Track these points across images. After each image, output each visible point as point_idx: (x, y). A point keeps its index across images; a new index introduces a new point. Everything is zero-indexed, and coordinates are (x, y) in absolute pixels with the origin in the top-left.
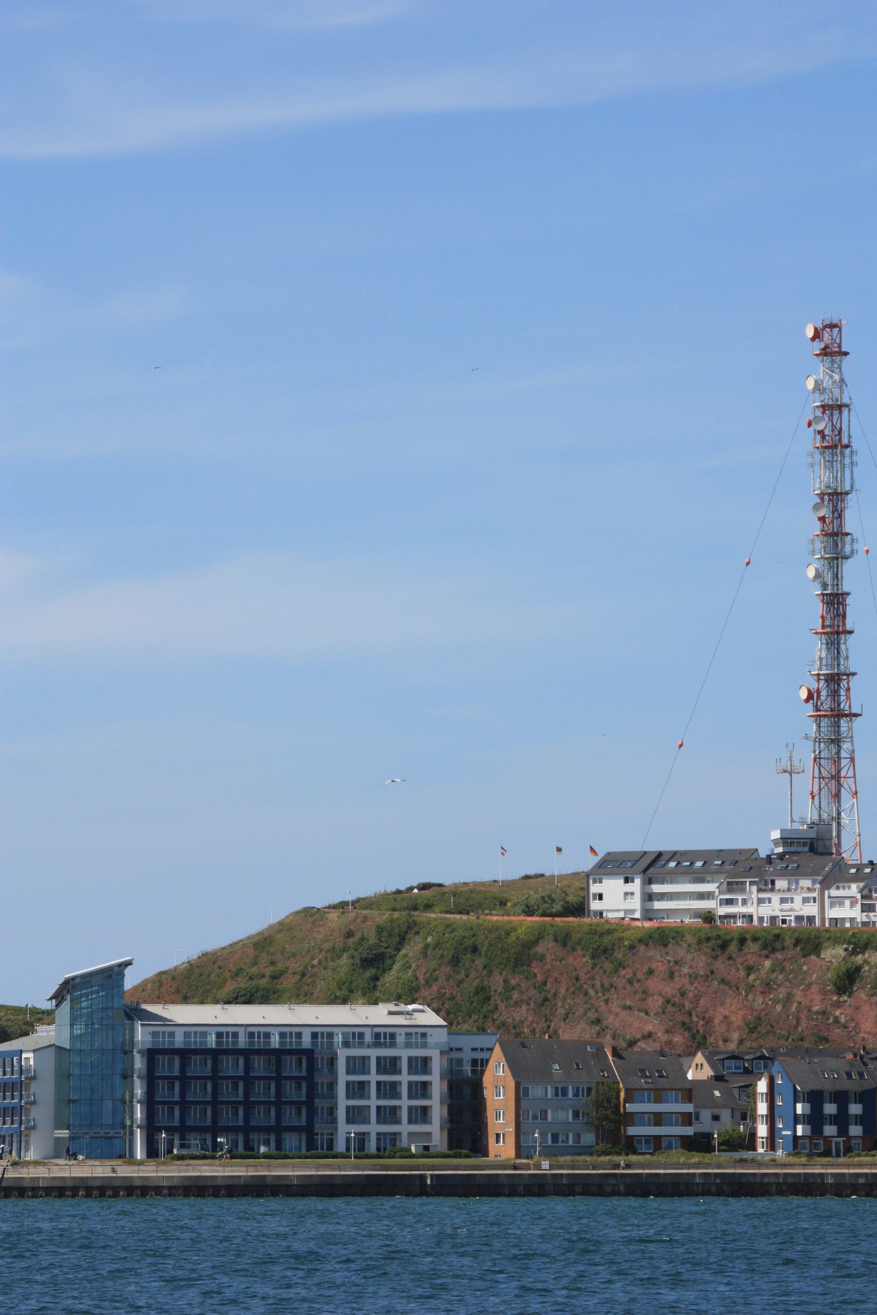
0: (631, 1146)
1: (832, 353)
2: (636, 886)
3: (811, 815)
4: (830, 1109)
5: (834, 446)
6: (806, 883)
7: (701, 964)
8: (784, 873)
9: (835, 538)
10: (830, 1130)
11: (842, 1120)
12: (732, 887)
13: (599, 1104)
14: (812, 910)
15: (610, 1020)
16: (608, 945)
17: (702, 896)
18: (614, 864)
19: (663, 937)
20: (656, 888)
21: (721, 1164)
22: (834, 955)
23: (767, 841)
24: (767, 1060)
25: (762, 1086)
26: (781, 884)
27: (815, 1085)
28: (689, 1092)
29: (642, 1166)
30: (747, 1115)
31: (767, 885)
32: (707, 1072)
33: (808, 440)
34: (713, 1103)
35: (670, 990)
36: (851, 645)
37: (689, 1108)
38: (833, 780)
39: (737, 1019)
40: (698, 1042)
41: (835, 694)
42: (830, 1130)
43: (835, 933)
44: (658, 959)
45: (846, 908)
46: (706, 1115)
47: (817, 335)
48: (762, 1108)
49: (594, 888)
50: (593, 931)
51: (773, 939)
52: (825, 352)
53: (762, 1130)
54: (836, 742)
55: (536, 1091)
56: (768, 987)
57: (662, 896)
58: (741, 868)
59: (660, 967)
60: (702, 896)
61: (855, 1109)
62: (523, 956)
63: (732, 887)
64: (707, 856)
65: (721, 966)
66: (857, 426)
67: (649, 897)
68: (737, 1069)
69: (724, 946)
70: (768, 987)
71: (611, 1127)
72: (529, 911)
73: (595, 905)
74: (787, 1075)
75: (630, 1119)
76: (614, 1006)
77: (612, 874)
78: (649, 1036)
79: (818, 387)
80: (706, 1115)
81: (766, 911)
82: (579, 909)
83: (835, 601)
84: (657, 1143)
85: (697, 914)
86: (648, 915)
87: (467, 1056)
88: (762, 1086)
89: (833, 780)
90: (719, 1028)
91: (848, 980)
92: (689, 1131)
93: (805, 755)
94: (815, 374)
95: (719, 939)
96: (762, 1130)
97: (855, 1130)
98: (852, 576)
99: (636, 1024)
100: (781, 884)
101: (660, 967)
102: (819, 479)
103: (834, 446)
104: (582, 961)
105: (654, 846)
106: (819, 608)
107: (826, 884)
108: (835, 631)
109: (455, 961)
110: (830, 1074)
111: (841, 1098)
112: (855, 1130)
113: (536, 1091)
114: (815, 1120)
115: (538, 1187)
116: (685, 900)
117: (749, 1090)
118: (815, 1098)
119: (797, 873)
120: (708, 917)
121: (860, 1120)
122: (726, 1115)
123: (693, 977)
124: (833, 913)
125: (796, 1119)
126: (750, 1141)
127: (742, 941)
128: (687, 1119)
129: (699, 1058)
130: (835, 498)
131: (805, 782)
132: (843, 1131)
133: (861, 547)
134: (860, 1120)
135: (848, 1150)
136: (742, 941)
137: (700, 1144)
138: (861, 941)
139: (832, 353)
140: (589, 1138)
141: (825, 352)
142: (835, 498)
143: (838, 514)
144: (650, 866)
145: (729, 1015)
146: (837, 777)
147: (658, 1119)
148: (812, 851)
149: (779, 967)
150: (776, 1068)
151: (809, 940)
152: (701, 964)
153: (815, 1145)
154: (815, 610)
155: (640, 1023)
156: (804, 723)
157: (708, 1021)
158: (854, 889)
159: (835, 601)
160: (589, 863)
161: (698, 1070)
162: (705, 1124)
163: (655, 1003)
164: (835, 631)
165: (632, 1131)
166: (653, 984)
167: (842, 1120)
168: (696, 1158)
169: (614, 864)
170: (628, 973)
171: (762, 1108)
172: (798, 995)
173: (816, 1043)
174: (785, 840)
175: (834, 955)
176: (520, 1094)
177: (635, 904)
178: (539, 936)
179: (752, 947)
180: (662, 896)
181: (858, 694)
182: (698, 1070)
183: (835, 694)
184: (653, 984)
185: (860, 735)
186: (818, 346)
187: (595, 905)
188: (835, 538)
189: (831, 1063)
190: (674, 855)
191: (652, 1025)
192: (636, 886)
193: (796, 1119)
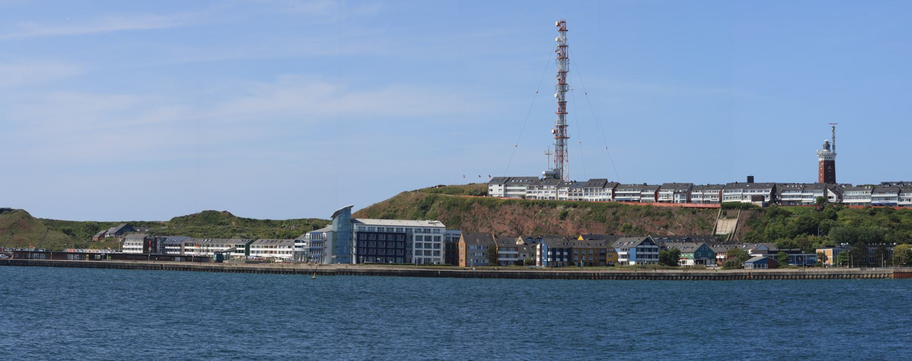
0: (499, 264)
1: (563, 30)
2: (502, 187)
3: (554, 167)
4: (558, 253)
5: (563, 58)
6: (552, 187)
7: (521, 210)
8: (546, 184)
9: (563, 85)
10: (558, 260)
11: (561, 257)
12: (530, 188)
13: (490, 251)
14: (554, 195)
15: (494, 227)
16: (494, 204)
17: (522, 190)
18: (496, 181)
19: (510, 203)
20: (508, 188)
21: (526, 269)
22: (560, 208)
23: (541, 175)
24: (539, 239)
25: (538, 247)
26: (545, 187)
27: (554, 247)
28: (517, 248)
29: (503, 269)
30: (534, 255)
31: (541, 188)
32: (522, 242)
33: (555, 56)
34: (524, 251)
35: (512, 218)
36: (567, 117)
37: (516, 253)
38: (561, 157)
39: (531, 227)
40: (520, 233)
41: (562, 131)
42: (558, 260)
43: (561, 202)
44: (508, 209)
45: (564, 195)
46: (521, 255)
47: (559, 25)
48: (538, 253)
49: (490, 188)
50: (489, 200)
51: (542, 204)
52: (561, 30)
53: (538, 260)
54: (562, 146)
55: (472, 247)
56: (541, 217)
57: (510, 190)
58: (533, 182)
59: (509, 211)
60: (522, 190)
61: (565, 253)
62: (468, 207)
63: (530, 188)
64: (523, 179)
65: (527, 211)
66: (570, 52)
67: (506, 191)
68: (531, 241)
69: (528, 205)
70: (541, 217)
71: (494, 258)
72: (471, 194)
73: (490, 193)
74: (546, 243)
75: (499, 256)
76: (495, 222)
77: (495, 184)
78: (505, 231)
79: (559, 40)
80: (521, 255)
81: (540, 195)
82: (486, 194)
83: (563, 104)
84: (507, 263)
85: (520, 196)
86: (506, 195)
87: (451, 236)
88: (538, 247)
89: (561, 157)
90: (526, 229)
91: (564, 216)
92: (517, 259)
93: (553, 149)
94: (558, 36)
95: (526, 203)
96: (538, 260)
97: (565, 260)
98: (568, 97)
99: (502, 228)
100: (545, 187)
101: (509, 211)
102: (558, 67)
103: (563, 58)
104: (486, 209)
105: (508, 176)
106: (558, 106)
107: (558, 187)
108: (562, 113)
109: (449, 208)
110: (558, 243)
111: (561, 250)
112: (565, 260)
113: (472, 247)
114: (554, 257)
115: (471, 275)
116: (516, 192)
117: (534, 248)
118: (554, 250)
119: (549, 184)
120: (523, 197)
121: (567, 257)
122: (527, 255)
123: (519, 214)
124: (560, 196)
125: (548, 256)
126: (534, 263)
127: (533, 204)
128: (516, 256)
129: (520, 238)
130: (563, 73)
131: (553, 157)
132: (562, 260)
133: (570, 88)
134: (567, 257)
135: (563, 265)
136: (533, 204)
137: (520, 263)
138: (568, 204)
139: (563, 30)
140: (487, 261)
141: (561, 30)
142: (563, 73)
143: (564, 78)
144: (506, 182)
145: (529, 226)
146: (562, 156)
147: (507, 256)
148: (554, 178)
149: (544, 212)
150: (542, 241)
151: (553, 204)
152: (521, 210)
153: (554, 264)
154: (557, 106)
155: (503, 227)
156: (553, 140)
157: (523, 227)
158: (566, 189)
159: (563, 104)
160: (488, 180)
161: (520, 242)
162: (521, 257)
163: (507, 222)
164: (562, 113)
165: (500, 259)
166: (507, 216)
167: (561, 257)
168: (518, 267)
169: (496, 181)
170: (499, 213)
171: (538, 253)
172: (549, 220)
173: (555, 234)
174: (546, 174)
175: (560, 208)
176: (467, 248)
177: (502, 192)
178: (473, 201)
179: (536, 206)
180: (510, 190)
181: (569, 132)
182: (520, 242)
183: (562, 131)
184: (507, 216)
185: (570, 144)
186: (559, 28)
187: (490, 193)
188: (563, 85)
189: (559, 240)
190: (514, 178)
191: (506, 228)
192: (502, 187)
193: (548, 256)
